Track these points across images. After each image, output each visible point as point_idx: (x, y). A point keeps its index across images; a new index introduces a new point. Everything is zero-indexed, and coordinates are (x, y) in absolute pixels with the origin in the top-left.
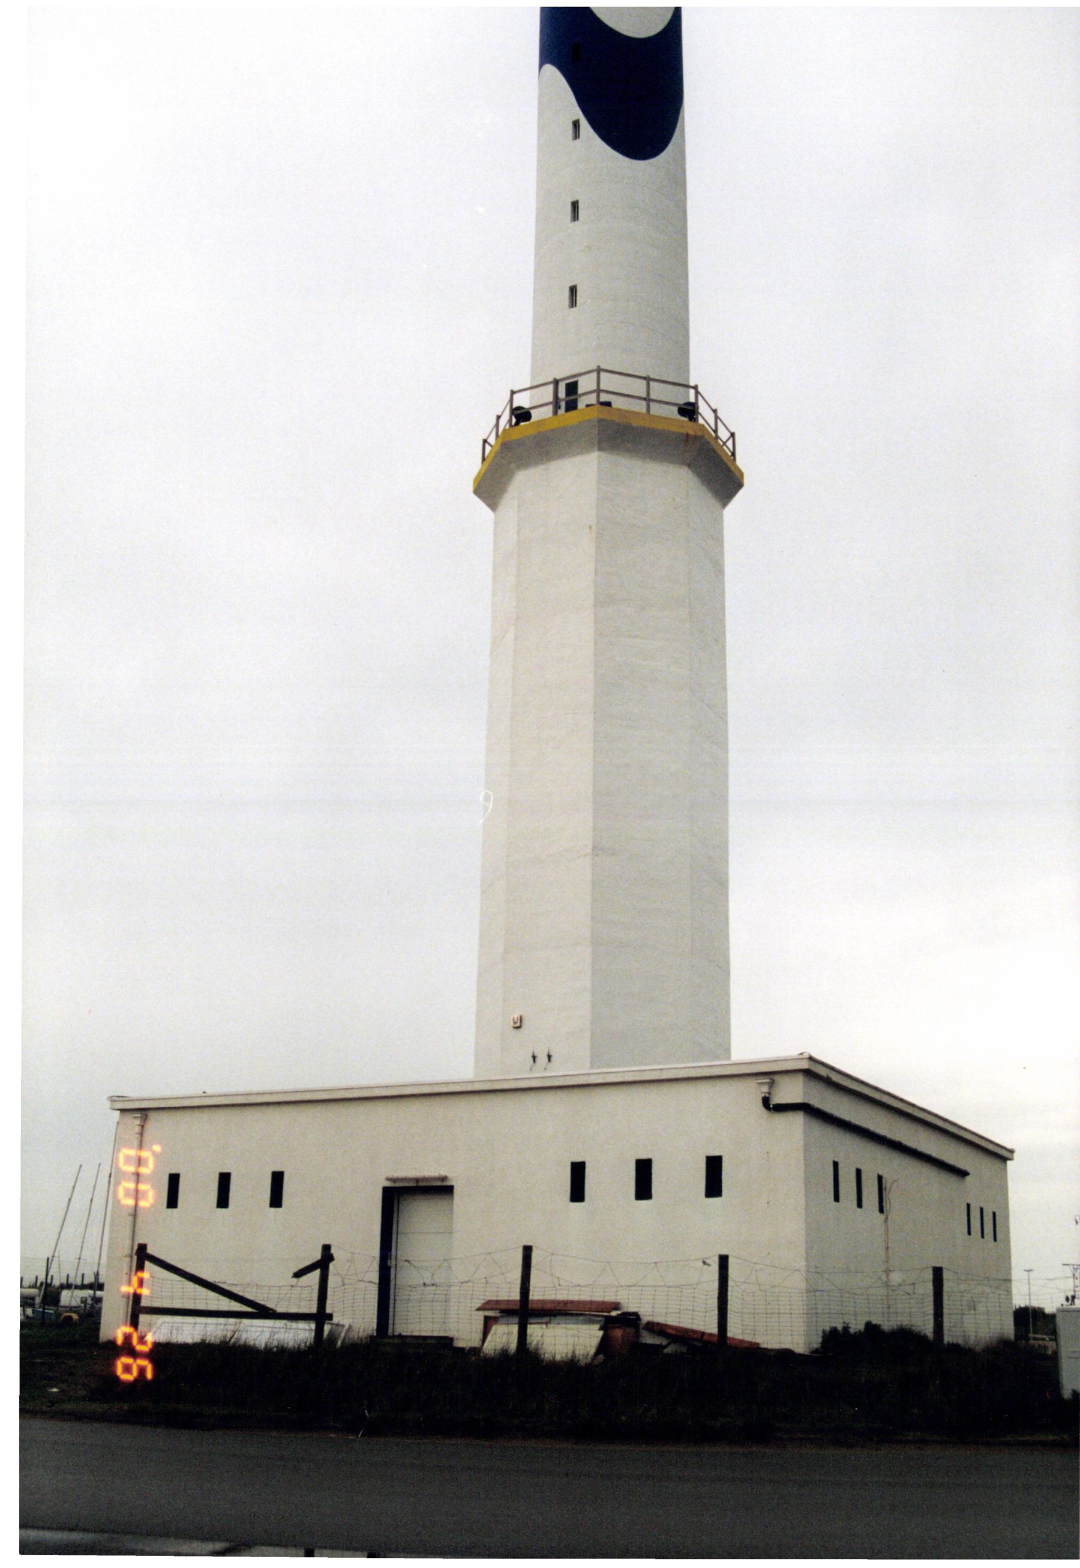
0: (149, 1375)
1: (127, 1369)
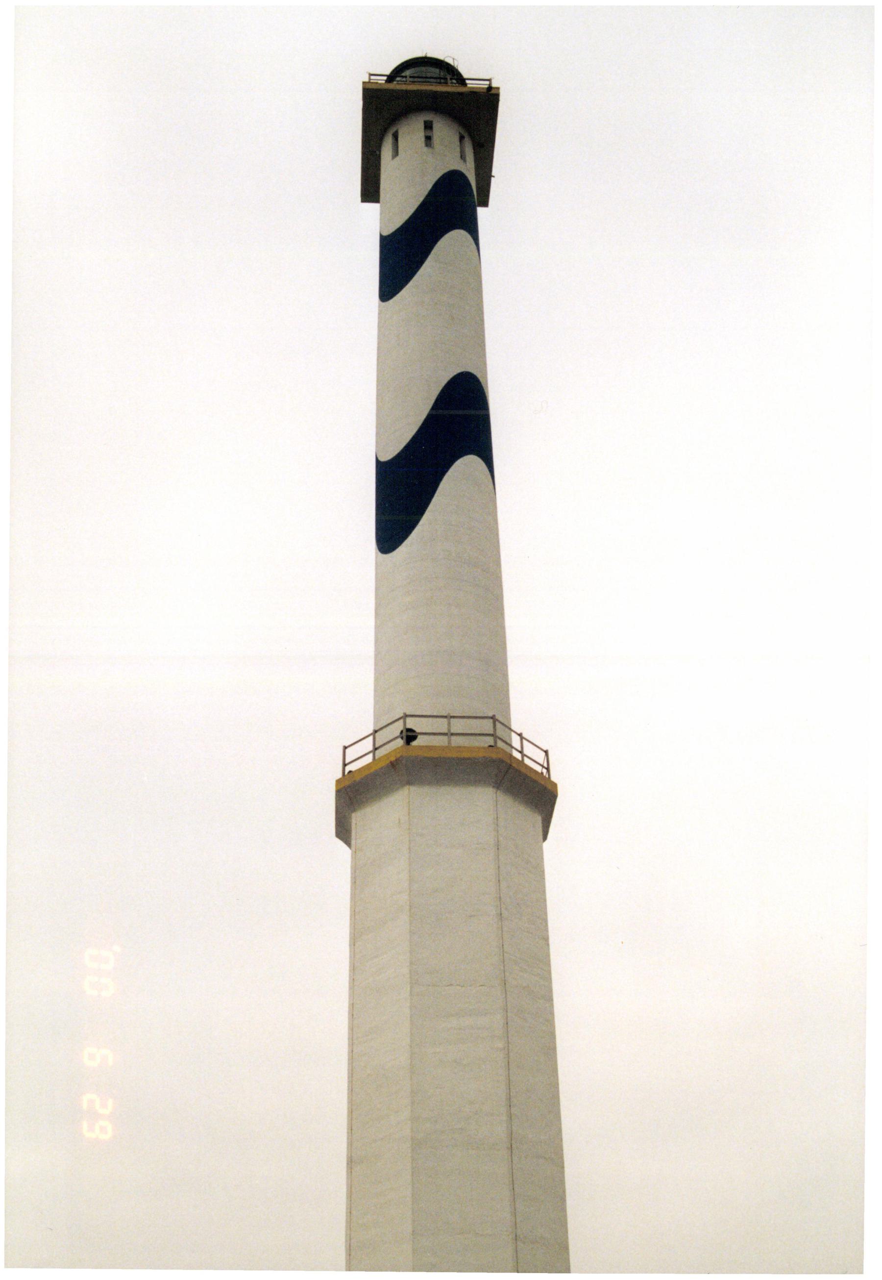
0: (85, 1125)
1: (103, 1130)
